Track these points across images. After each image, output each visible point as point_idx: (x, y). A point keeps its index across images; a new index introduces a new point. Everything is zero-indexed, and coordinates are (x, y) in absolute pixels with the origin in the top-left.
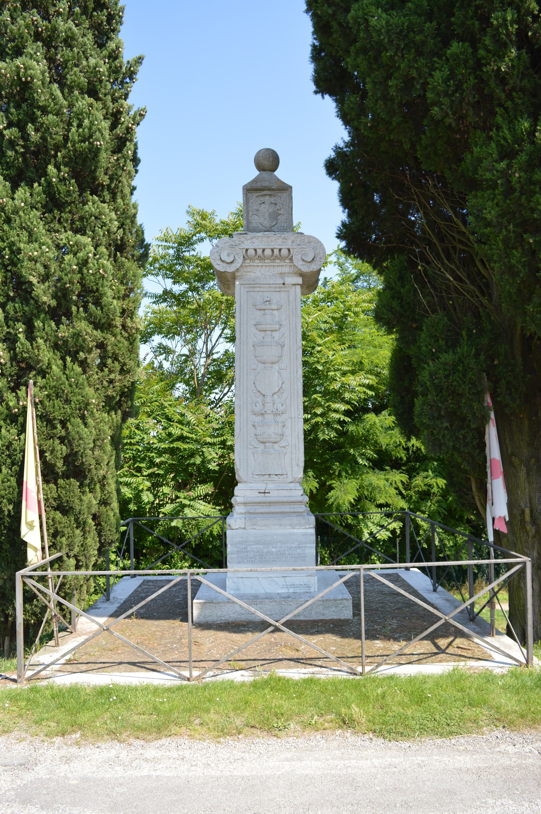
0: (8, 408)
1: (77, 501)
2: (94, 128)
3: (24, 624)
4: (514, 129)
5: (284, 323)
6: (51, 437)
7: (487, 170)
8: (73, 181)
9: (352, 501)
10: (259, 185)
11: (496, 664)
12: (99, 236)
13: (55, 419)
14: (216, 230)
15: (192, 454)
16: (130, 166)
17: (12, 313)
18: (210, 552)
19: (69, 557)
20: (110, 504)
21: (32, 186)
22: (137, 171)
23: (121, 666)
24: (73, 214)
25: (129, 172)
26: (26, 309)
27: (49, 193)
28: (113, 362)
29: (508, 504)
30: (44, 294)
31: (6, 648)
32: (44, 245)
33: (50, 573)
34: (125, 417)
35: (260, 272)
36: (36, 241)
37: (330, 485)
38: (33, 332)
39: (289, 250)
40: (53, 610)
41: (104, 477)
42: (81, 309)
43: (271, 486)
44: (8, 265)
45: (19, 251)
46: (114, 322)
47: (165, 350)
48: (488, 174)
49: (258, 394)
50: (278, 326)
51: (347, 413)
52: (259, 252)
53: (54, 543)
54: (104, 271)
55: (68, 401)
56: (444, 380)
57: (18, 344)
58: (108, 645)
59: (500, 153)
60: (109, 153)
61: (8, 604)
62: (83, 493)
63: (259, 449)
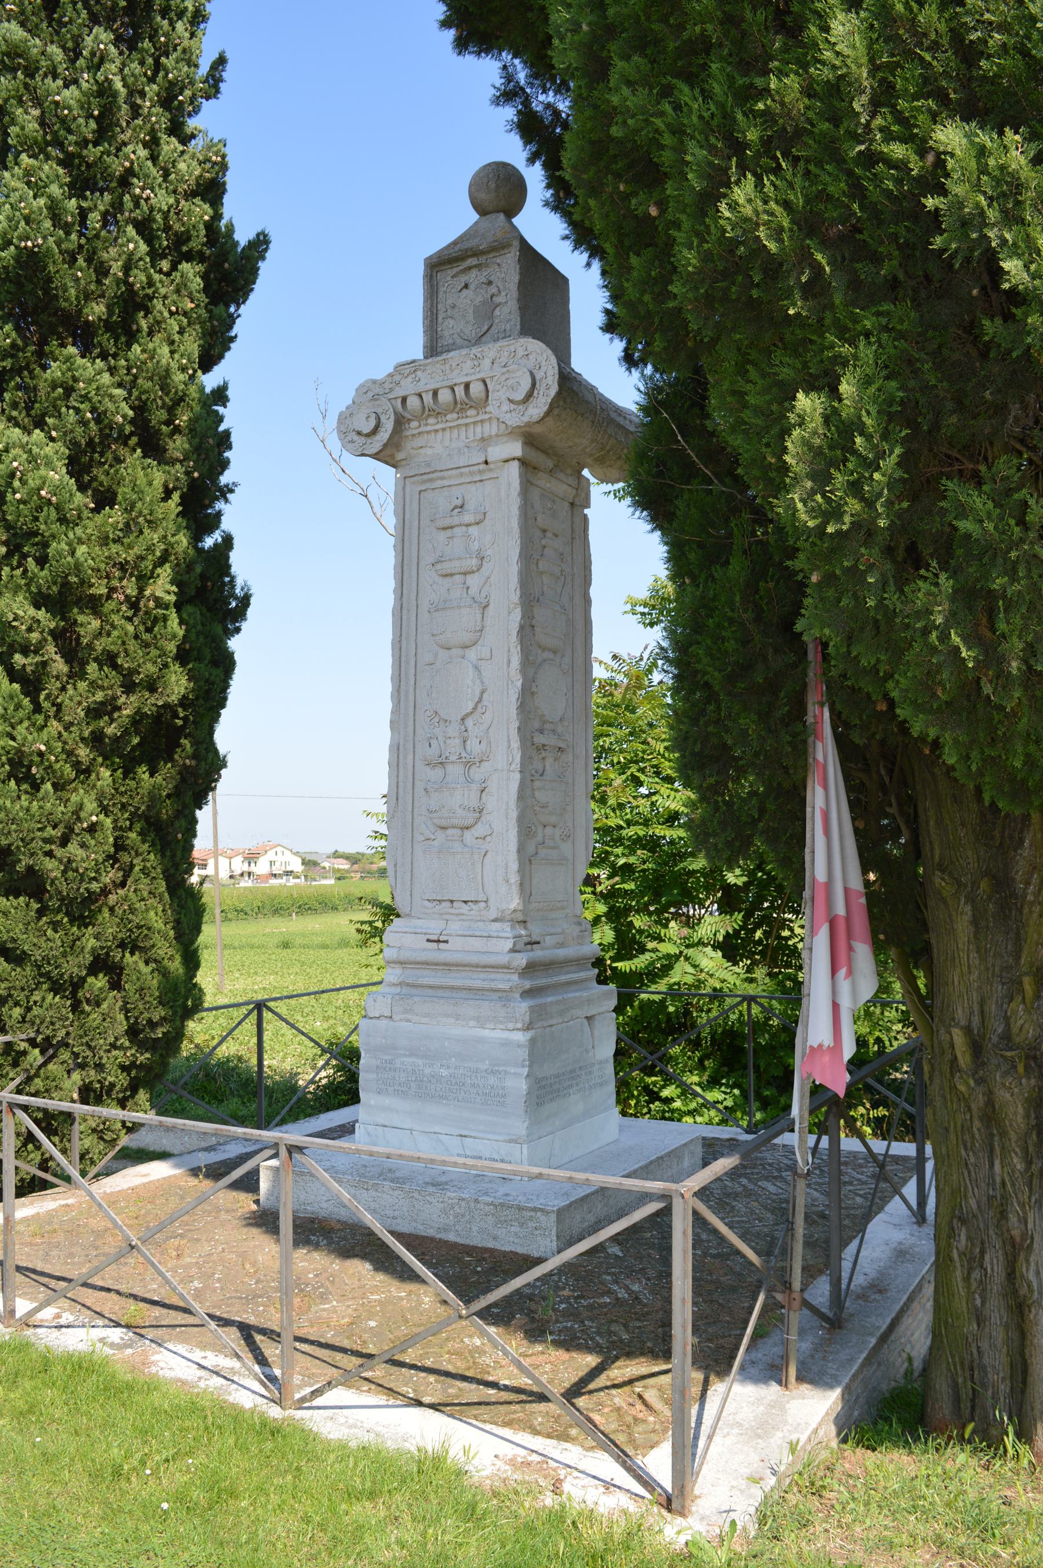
5: (489, 552)
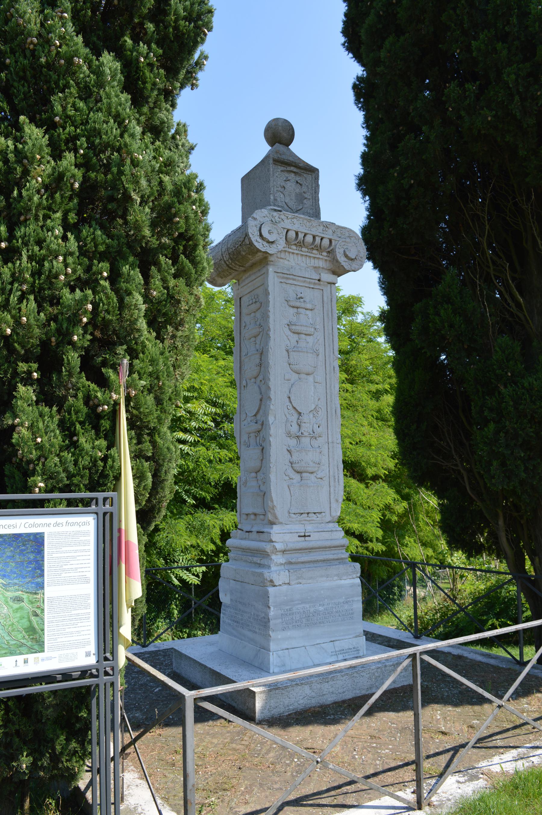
43: (309, 528)
49: (293, 411)
50: (313, 330)
63: (294, 481)
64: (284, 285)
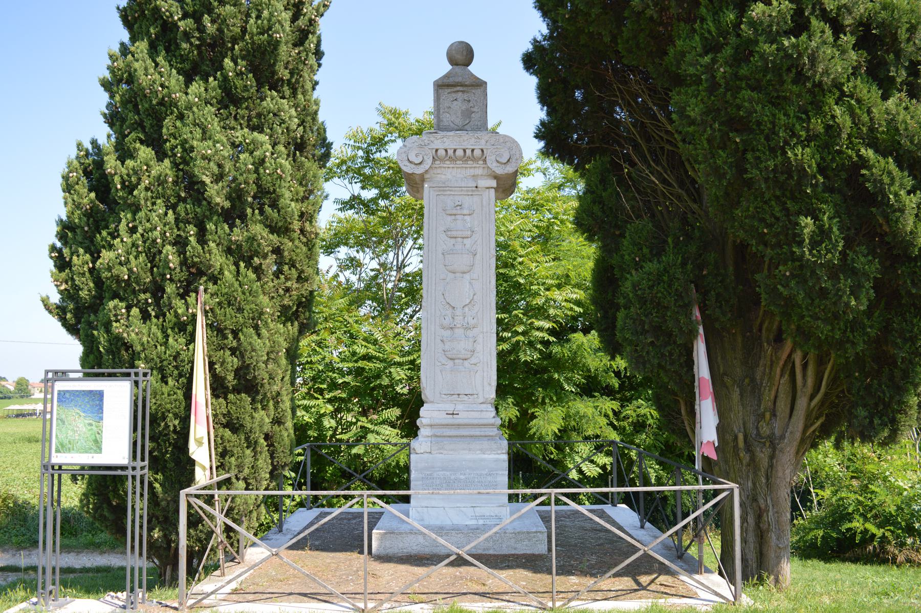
0: (177, 315)
1: (248, 419)
2: (274, 19)
3: (188, 551)
4: (719, 22)
6: (222, 348)
7: (691, 65)
8: (251, 75)
9: (557, 431)
10: (451, 80)
11: (701, 602)
12: (278, 133)
13: (226, 328)
14: (410, 129)
15: (378, 376)
16: (312, 60)
17: (183, 214)
18: (394, 481)
19: (238, 479)
20: (284, 423)
21: (207, 81)
22: (320, 65)
23: (291, 597)
24: (251, 111)
25: (311, 67)
26: (198, 210)
27: (225, 88)
28: (290, 269)
29: (718, 428)
30: (217, 195)
31: (167, 578)
32: (218, 142)
33: (216, 492)
34: (301, 332)
35: (450, 174)
36: (210, 139)
37: (533, 413)
38: (204, 235)
39: (482, 151)
40: (219, 535)
41: (278, 394)
42: (257, 211)
43: (460, 407)
44: (180, 164)
45: (192, 149)
46: (291, 226)
47: (353, 264)
48: (691, 69)
49: (448, 306)
50: (469, 233)
51: (551, 332)
52: (450, 152)
53: (222, 463)
54: (282, 171)
55: (240, 310)
56: (648, 291)
57: (189, 247)
58: (278, 576)
59: (704, 47)
60: (290, 45)
61: (171, 529)
62: (255, 409)
64: (442, 197)
